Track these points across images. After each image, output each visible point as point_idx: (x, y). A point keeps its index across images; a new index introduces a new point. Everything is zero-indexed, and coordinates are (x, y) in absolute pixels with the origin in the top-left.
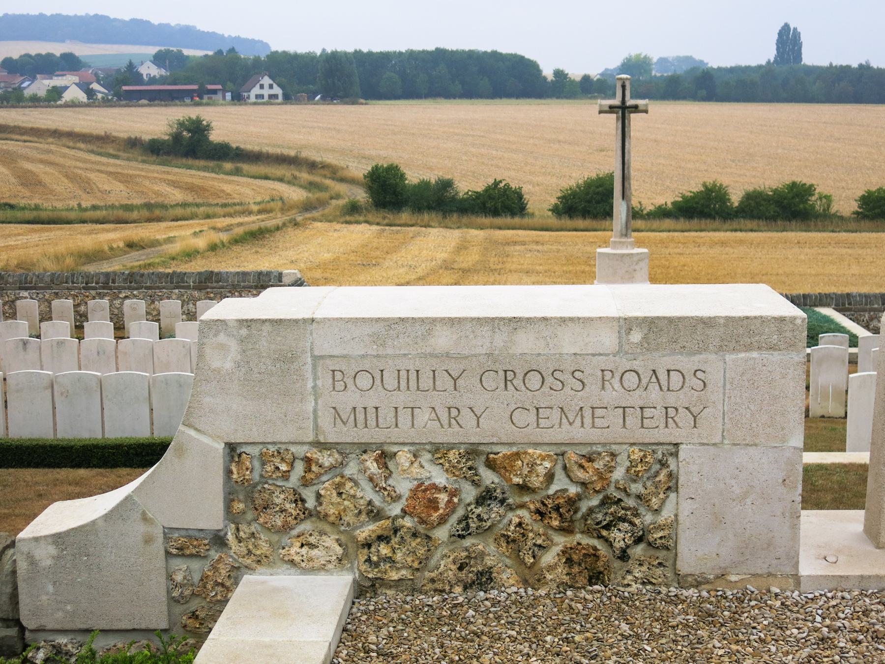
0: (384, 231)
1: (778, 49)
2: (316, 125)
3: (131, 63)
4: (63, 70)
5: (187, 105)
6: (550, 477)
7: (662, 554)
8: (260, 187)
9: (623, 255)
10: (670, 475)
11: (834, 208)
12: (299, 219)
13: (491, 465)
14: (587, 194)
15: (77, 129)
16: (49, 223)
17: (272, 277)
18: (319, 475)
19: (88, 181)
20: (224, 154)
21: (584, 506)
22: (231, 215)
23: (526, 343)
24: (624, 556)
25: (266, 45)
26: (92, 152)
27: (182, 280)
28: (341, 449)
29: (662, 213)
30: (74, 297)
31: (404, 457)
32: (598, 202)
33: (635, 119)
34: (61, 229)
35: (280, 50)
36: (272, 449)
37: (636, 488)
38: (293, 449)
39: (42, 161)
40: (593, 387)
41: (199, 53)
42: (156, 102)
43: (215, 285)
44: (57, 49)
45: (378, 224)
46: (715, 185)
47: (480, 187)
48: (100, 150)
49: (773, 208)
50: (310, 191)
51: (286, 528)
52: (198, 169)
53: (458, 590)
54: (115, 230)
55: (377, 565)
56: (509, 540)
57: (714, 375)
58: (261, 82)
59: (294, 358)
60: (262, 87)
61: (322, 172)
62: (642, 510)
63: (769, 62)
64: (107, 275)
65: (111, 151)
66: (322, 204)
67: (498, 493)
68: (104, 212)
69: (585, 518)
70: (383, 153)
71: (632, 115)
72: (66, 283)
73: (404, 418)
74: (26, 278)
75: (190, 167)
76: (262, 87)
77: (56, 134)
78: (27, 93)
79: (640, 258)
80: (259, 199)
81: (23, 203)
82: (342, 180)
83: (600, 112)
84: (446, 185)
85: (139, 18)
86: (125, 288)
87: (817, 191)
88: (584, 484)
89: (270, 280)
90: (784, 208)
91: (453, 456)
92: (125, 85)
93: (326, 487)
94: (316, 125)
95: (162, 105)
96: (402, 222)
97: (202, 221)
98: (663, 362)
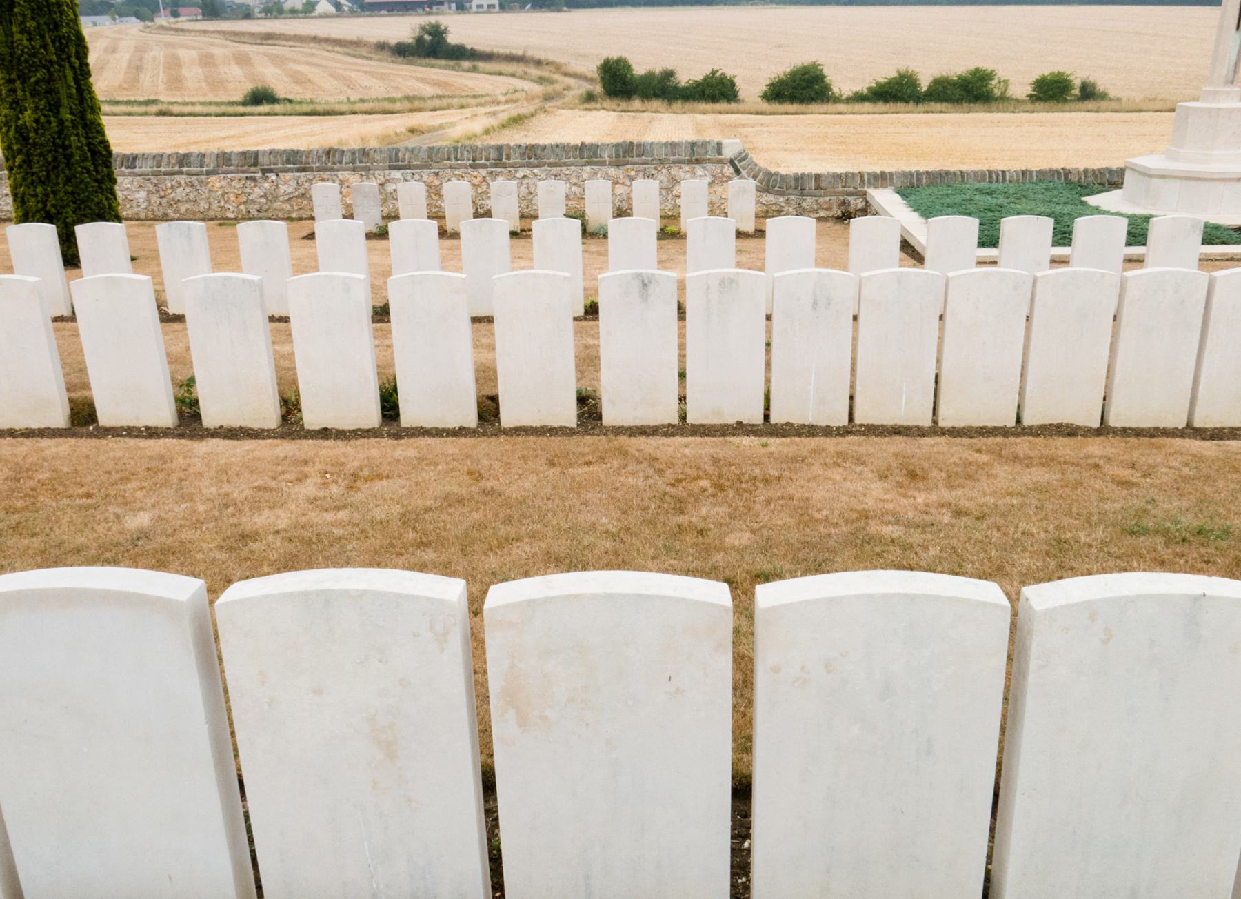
11: (1009, 93)
17: (709, 148)
20: (459, 54)
26: (349, 54)
27: (595, 155)
29: (859, 98)
32: (804, 89)
39: (308, 63)
43: (636, 159)
47: (699, 77)
52: (440, 67)
64: (499, 149)
72: (448, 159)
74: (397, 154)
75: (433, 66)
77: (315, 39)
81: (298, 98)
82: (566, 74)
86: (523, 166)
89: (706, 153)
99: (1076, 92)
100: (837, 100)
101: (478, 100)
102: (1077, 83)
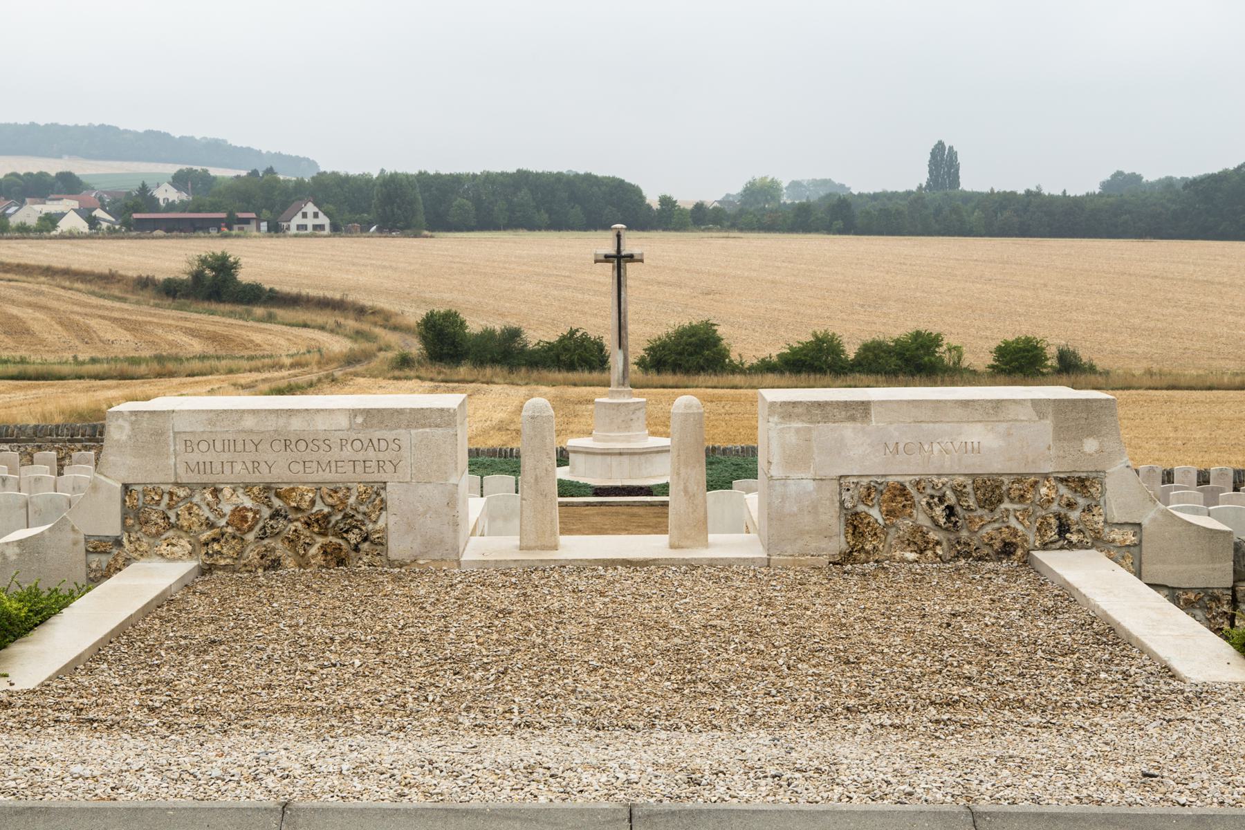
0: (437, 387)
1: (931, 172)
2: (369, 262)
3: (144, 185)
4: (59, 192)
5: (212, 237)
6: (313, 502)
7: (379, 548)
8: (296, 336)
9: (619, 404)
10: (382, 500)
12: (338, 374)
13: (278, 495)
14: (677, 345)
15: (75, 266)
16: (37, 378)
18: (177, 503)
19: (88, 329)
20: (254, 296)
21: (333, 520)
22: (258, 370)
23: (296, 424)
24: (356, 549)
25: (313, 164)
28: (191, 487)
30: (58, 450)
31: (227, 491)
32: (691, 354)
33: (630, 268)
34: (52, 386)
35: (329, 170)
36: (150, 487)
37: (362, 508)
38: (162, 487)
39: (29, 305)
40: (336, 449)
41: (229, 173)
42: (174, 233)
44: (52, 167)
45: (432, 380)
46: (826, 334)
48: (105, 292)
49: (894, 361)
50: (356, 341)
51: (158, 534)
53: (260, 571)
54: (117, 387)
55: (212, 556)
56: (291, 541)
57: (405, 443)
58: (304, 210)
59: (162, 434)
60: (305, 215)
61: (371, 318)
62: (367, 522)
63: (920, 188)
65: (117, 293)
66: (367, 356)
67: (283, 512)
68: (105, 366)
69: (334, 526)
70: (447, 296)
71: (628, 265)
73: (227, 467)
75: (213, 313)
76: (305, 215)
77: (49, 272)
78: (14, 221)
79: (638, 407)
80: (293, 351)
82: (395, 328)
83: (596, 261)
84: (513, 334)
87: (945, 342)
88: (332, 506)
90: (907, 361)
91: (255, 490)
92: (136, 212)
93: (181, 509)
94: (369, 262)
95: (181, 237)
96: (461, 377)
97: (223, 377)
98: (378, 434)
99: (1052, 362)
100: (735, 369)
101: (253, 363)
102: (1052, 352)
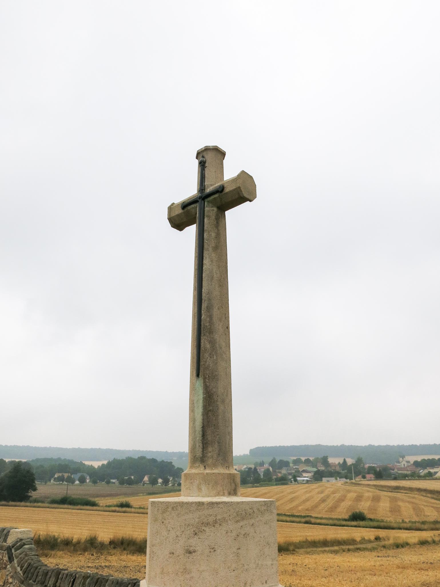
26: (433, 498)
77: (419, 490)
85: (414, 444)
